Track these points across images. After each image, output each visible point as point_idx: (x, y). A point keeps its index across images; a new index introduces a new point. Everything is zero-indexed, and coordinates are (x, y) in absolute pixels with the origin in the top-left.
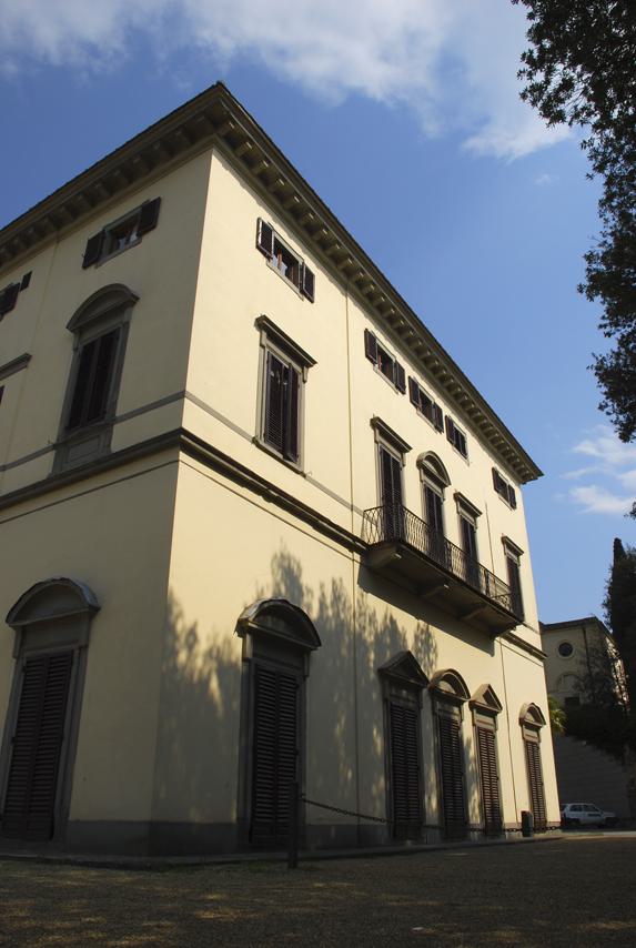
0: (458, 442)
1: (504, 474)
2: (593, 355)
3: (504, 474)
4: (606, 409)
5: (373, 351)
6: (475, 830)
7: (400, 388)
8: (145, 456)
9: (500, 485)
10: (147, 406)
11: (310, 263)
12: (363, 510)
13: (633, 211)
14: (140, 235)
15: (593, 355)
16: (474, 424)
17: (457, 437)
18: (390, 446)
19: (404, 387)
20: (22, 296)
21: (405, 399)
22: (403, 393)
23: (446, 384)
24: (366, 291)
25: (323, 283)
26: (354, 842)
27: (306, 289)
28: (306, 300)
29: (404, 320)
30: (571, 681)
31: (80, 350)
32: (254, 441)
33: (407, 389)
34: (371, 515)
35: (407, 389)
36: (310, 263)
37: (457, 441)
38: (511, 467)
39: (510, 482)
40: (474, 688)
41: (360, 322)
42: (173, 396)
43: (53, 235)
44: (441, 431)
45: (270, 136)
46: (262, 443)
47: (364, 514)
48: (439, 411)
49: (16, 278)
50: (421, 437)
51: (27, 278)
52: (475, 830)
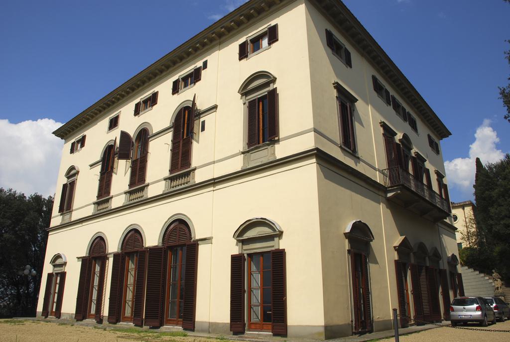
1: (433, 137)
2: (499, 87)
3: (433, 137)
4: (508, 119)
6: (110, 254)
12: (381, 169)
14: (270, 44)
15: (499, 87)
20: (203, 72)
25: (355, 57)
26: (385, 326)
28: (349, 67)
31: (247, 104)
32: (341, 147)
34: (386, 172)
38: (436, 133)
40: (428, 246)
42: (328, 138)
43: (218, 41)
46: (343, 146)
49: (199, 64)
51: (205, 65)
52: (110, 254)
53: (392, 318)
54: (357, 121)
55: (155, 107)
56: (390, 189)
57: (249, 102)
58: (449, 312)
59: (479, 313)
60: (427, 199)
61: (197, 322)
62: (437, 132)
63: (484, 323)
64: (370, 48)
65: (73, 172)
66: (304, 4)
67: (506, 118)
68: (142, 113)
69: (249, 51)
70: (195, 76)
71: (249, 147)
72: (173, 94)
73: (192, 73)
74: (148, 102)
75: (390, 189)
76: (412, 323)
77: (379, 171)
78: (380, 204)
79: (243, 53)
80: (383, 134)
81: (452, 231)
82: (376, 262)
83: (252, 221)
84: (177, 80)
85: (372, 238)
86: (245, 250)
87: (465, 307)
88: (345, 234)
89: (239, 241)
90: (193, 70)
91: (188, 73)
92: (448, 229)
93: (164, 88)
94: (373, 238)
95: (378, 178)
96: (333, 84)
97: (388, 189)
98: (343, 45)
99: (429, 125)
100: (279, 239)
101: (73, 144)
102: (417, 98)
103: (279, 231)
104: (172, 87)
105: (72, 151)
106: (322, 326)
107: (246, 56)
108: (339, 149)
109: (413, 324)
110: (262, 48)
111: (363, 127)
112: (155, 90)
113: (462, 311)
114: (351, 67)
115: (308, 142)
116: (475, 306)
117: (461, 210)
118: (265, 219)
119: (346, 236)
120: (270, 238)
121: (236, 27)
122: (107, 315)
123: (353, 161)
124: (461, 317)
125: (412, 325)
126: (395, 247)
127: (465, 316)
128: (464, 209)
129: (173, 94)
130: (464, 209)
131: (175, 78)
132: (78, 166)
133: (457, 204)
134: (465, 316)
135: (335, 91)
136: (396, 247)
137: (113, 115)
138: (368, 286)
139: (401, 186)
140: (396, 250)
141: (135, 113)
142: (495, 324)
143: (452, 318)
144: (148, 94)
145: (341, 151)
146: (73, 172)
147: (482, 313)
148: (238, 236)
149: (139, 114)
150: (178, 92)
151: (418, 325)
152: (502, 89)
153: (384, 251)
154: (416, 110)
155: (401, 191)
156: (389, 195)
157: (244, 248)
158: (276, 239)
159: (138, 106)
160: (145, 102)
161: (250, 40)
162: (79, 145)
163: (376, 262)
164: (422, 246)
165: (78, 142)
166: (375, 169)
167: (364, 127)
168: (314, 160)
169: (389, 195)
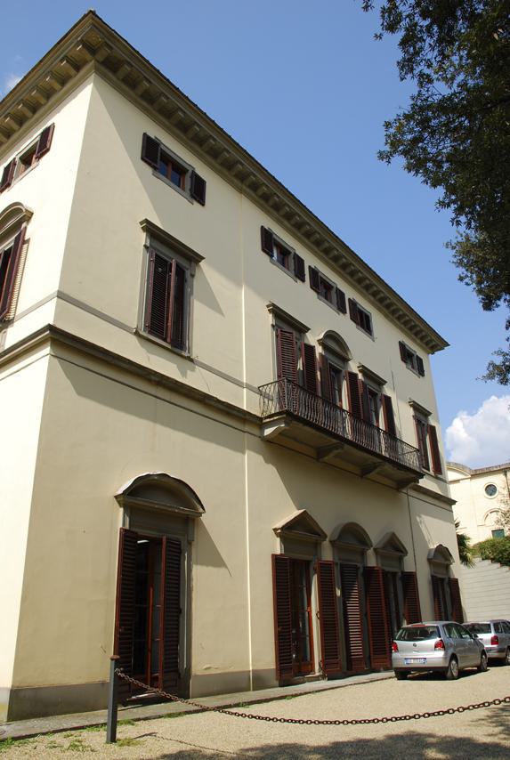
0: (363, 321)
1: (412, 346)
3: (412, 346)
5: (152, 154)
7: (299, 275)
8: (150, 381)
9: (407, 356)
10: (204, 365)
11: (203, 171)
12: (256, 386)
13: (509, 58)
16: (379, 305)
17: (361, 317)
18: (287, 327)
19: (345, 309)
21: (305, 288)
22: (303, 281)
23: (356, 278)
24: (260, 192)
25: (216, 186)
27: (198, 192)
28: (298, 281)
29: (255, 176)
30: (494, 516)
32: (137, 334)
33: (159, 154)
34: (264, 390)
35: (159, 154)
36: (203, 171)
37: (362, 321)
38: (418, 341)
39: (419, 352)
40: (375, 536)
41: (262, 219)
44: (344, 312)
45: (168, 77)
46: (142, 333)
47: (259, 391)
48: (341, 295)
50: (320, 320)
53: (251, 669)
54: (201, 301)
56: (268, 420)
58: (391, 652)
59: (440, 654)
60: (350, 438)
61: (196, 676)
62: (422, 339)
63: (449, 674)
67: (461, 279)
75: (268, 420)
76: (317, 674)
77: (249, 387)
78: (244, 453)
80: (273, 326)
81: (448, 507)
82: (217, 561)
85: (201, 510)
87: (416, 642)
88: (116, 497)
92: (436, 502)
94: (203, 508)
95: (246, 401)
96: (141, 223)
97: (264, 421)
98: (187, 167)
99: (402, 326)
102: (368, 276)
106: (7, 688)
108: (134, 339)
109: (318, 676)
111: (218, 315)
113: (410, 650)
114: (202, 203)
115: (45, 316)
116: (432, 642)
117: (501, 476)
119: (119, 502)
123: (175, 366)
124: (409, 661)
125: (317, 679)
126: (275, 530)
127: (416, 661)
128: (506, 475)
130: (506, 475)
133: (496, 467)
134: (416, 661)
135: (144, 235)
136: (278, 529)
138: (178, 600)
139: (284, 415)
140: (278, 535)
142: (486, 670)
143: (396, 664)
145: (139, 345)
147: (446, 654)
151: (330, 679)
152: (464, 234)
153: (245, 535)
154: (372, 298)
155: (286, 423)
156: (268, 432)
163: (217, 561)
164: (352, 535)
166: (239, 384)
167: (221, 312)
169: (268, 432)
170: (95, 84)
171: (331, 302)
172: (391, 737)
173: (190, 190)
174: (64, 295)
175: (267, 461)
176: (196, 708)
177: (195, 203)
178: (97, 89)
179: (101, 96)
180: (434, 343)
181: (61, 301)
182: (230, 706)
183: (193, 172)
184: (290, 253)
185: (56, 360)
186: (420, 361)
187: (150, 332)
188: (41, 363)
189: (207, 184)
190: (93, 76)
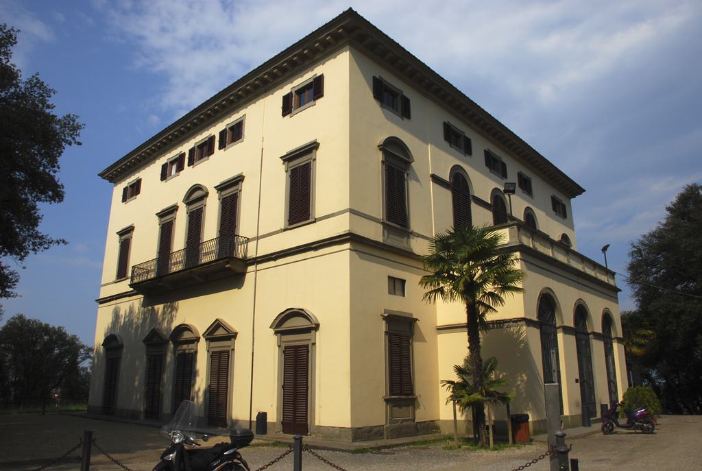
1: (560, 196)
3: (560, 196)
11: (408, 92)
31: (289, 172)
36: (408, 92)
55: (211, 157)
57: (292, 170)
64: (457, 102)
65: (198, 194)
66: (348, 52)
68: (198, 162)
69: (293, 105)
70: (236, 133)
71: (290, 224)
72: (284, 115)
73: (311, 83)
74: (204, 147)
79: (288, 108)
81: (612, 294)
83: (291, 311)
84: (289, 94)
86: (283, 342)
89: (276, 333)
90: (312, 80)
91: (306, 84)
93: (150, 175)
100: (316, 331)
101: (165, 167)
103: (315, 324)
104: (282, 106)
105: (164, 177)
107: (193, 164)
110: (171, 175)
112: (318, 71)
115: (341, 225)
118: (302, 310)
120: (307, 330)
121: (280, 74)
122: (558, 334)
129: (284, 115)
131: (287, 89)
132: (206, 185)
137: (131, 179)
141: (161, 178)
144: (307, 77)
146: (198, 194)
148: (277, 327)
149: (126, 201)
150: (225, 147)
157: (282, 340)
158: (313, 332)
159: (287, 100)
160: (300, 91)
161: (229, 128)
162: (174, 167)
165: (172, 163)
168: (348, 245)
170: (351, 52)
171: (460, 148)
172: (217, 445)
173: (402, 110)
174: (354, 210)
175: (154, 163)
176: (319, 452)
177: (405, 118)
178: (353, 55)
179: (354, 58)
180: (573, 189)
181: (352, 215)
182: (317, 448)
183: (402, 95)
184: (461, 136)
185: (354, 253)
186: (504, 165)
187: (389, 221)
188: (342, 256)
189: (411, 102)
190: (348, 47)
